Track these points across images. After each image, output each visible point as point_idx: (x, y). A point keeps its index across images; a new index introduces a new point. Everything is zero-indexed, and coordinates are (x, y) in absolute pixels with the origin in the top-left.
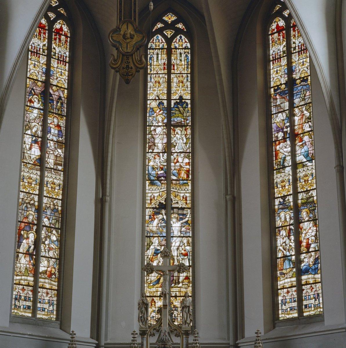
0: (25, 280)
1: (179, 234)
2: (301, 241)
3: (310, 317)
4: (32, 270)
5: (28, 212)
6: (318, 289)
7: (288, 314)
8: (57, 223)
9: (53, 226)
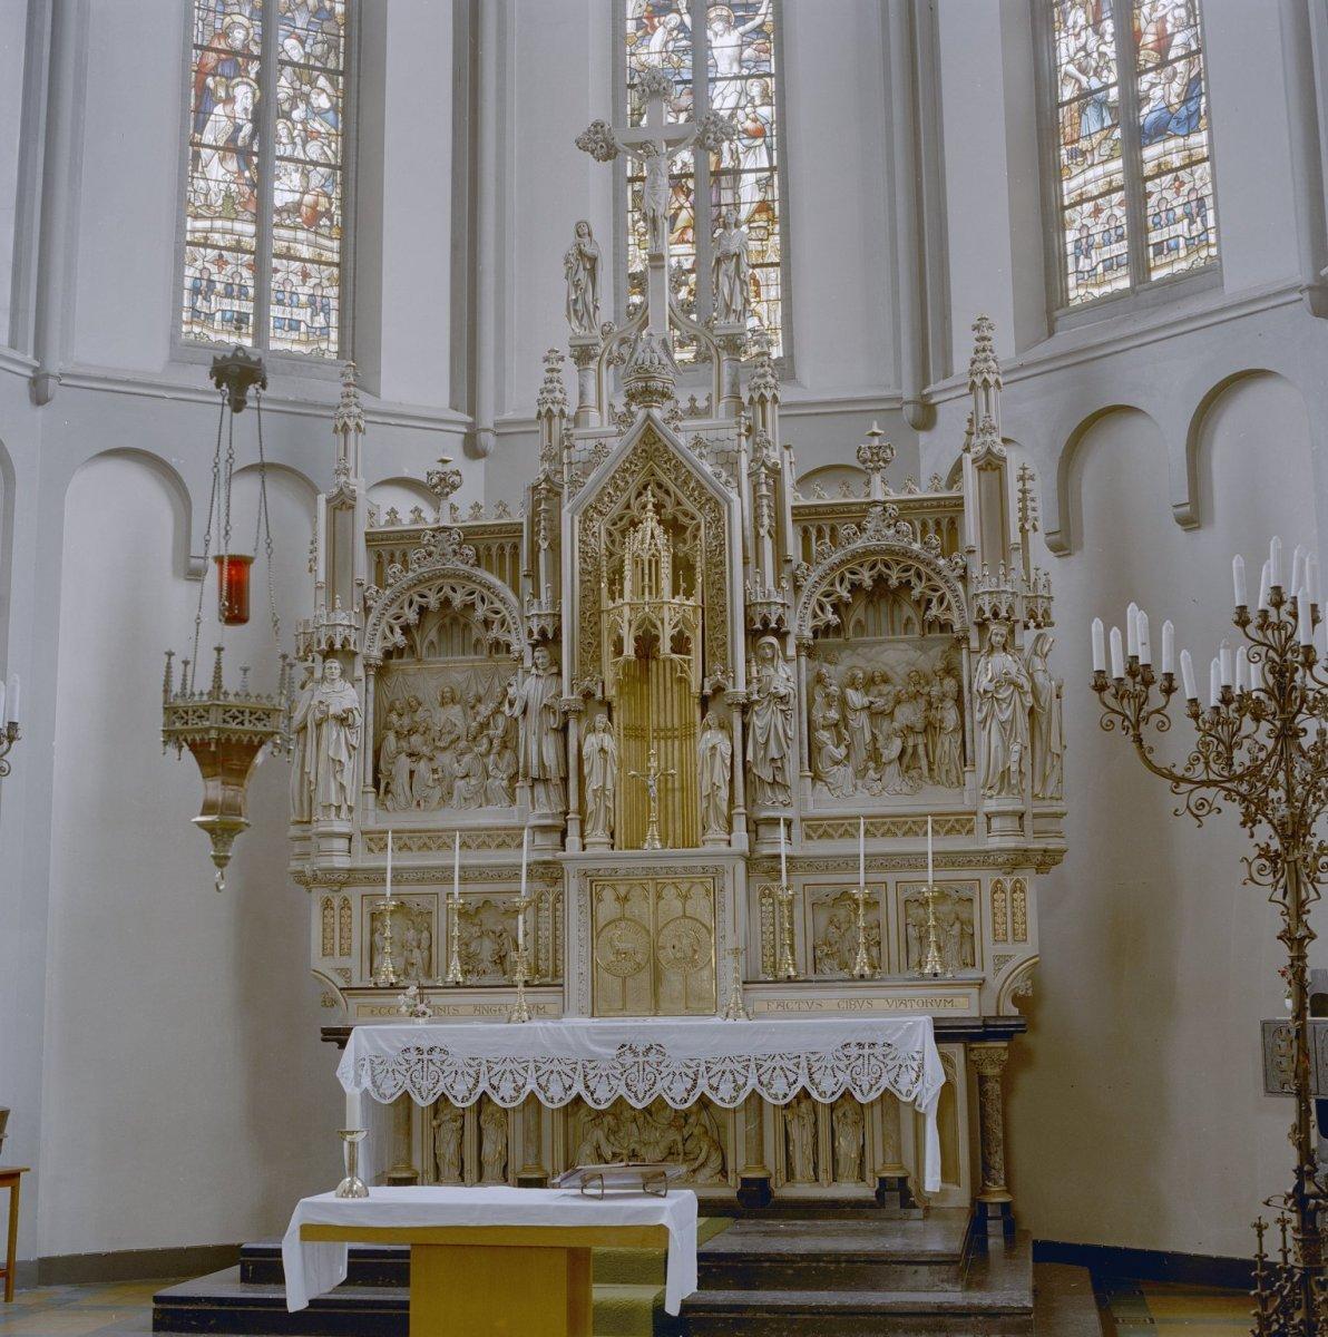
0: (225, 232)
1: (735, 69)
2: (1140, 30)
3: (1173, 280)
4: (249, 200)
5: (228, 19)
6: (1199, 184)
7: (1098, 285)
8: (332, 56)
9: (318, 64)
